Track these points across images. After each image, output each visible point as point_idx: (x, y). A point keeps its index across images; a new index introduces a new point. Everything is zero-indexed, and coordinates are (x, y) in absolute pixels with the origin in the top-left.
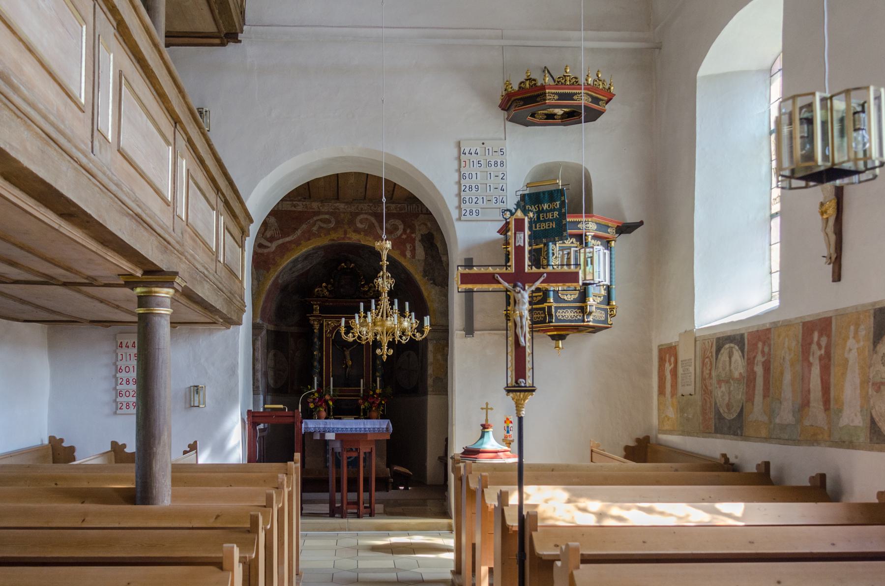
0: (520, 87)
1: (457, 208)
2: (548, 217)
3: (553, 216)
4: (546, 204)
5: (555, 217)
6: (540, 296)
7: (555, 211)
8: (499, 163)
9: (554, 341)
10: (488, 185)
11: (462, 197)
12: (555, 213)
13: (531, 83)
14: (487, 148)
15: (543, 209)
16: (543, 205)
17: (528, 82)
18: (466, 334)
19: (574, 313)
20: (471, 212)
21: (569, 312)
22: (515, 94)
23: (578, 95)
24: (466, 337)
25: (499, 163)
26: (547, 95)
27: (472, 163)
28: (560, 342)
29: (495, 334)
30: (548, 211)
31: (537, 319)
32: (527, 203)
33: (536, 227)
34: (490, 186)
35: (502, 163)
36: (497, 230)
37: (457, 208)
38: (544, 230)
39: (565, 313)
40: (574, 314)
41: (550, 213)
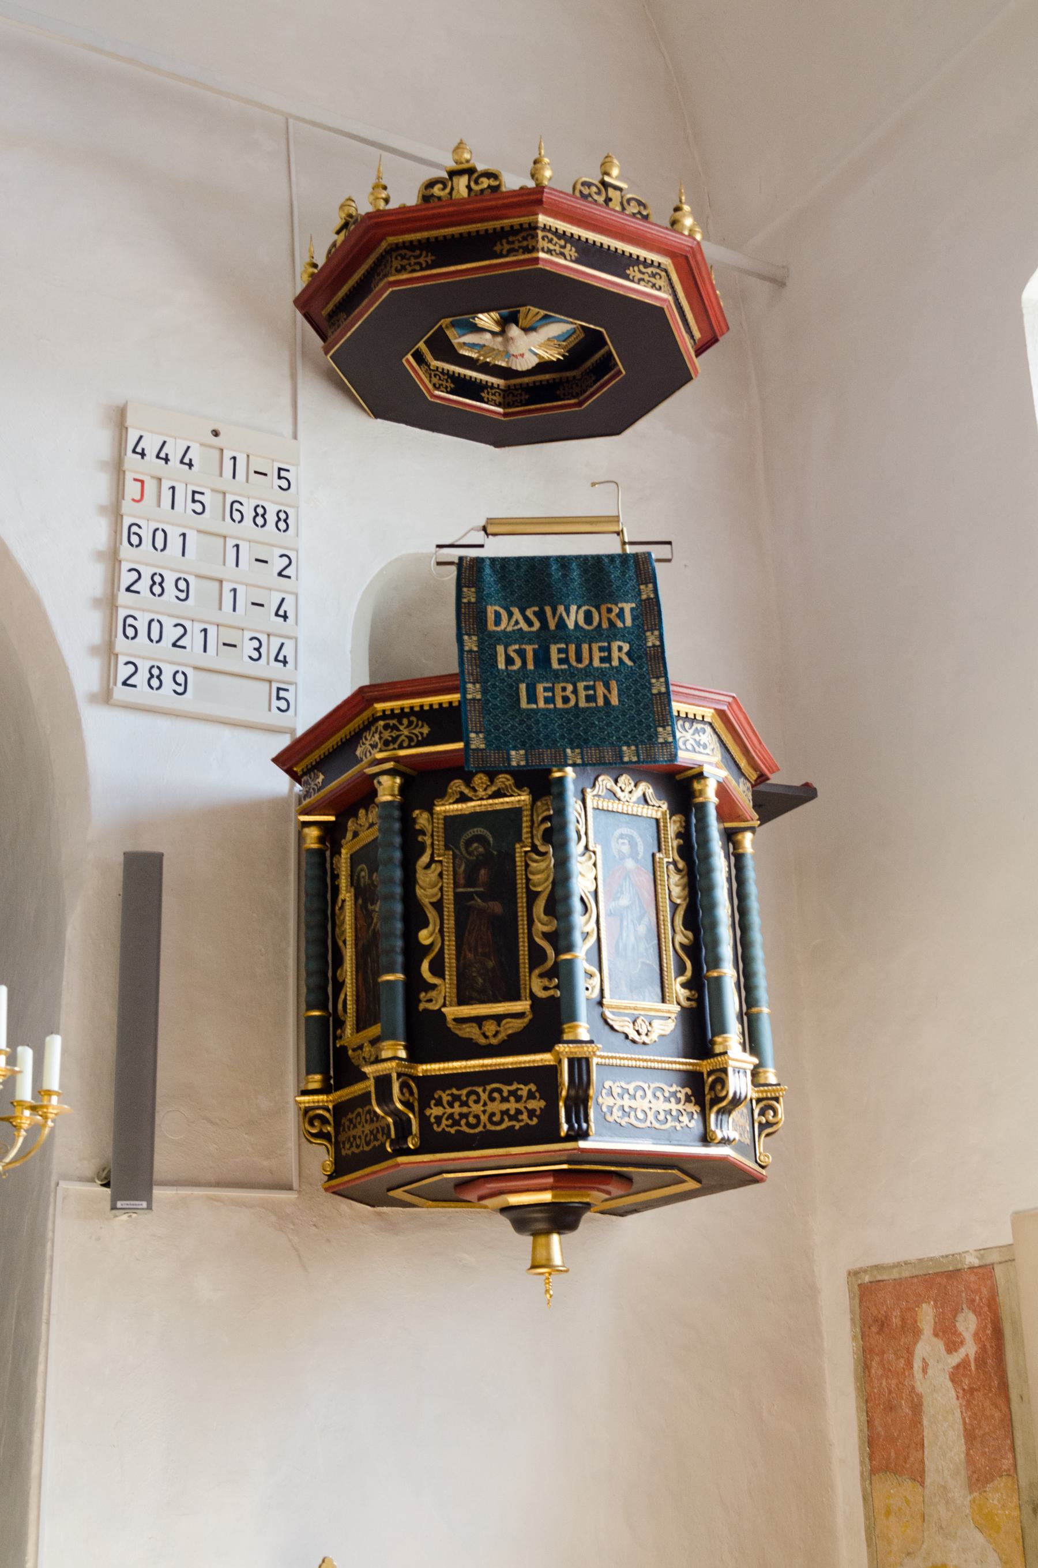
0: (426, 198)
1: (94, 650)
2: (586, 662)
3: (608, 659)
4: (573, 608)
5: (615, 663)
6: (520, 1015)
7: (615, 638)
8: (271, 518)
9: (528, 1239)
10: (227, 587)
11: (122, 613)
12: (615, 645)
13: (476, 182)
14: (228, 454)
15: (561, 624)
16: (561, 609)
17: (462, 182)
18: (114, 1199)
19: (667, 1100)
20: (155, 676)
21: (649, 1093)
22: (403, 219)
23: (641, 267)
24: (114, 1208)
25: (271, 518)
26: (540, 234)
27: (167, 495)
28: (555, 1238)
29: (235, 1202)
30: (581, 637)
31: (506, 1124)
32: (490, 596)
33: (532, 698)
34: (235, 590)
35: (283, 520)
36: (274, 754)
37: (94, 650)
38: (567, 711)
39: (464, 1104)
40: (667, 1106)
41: (595, 647)
